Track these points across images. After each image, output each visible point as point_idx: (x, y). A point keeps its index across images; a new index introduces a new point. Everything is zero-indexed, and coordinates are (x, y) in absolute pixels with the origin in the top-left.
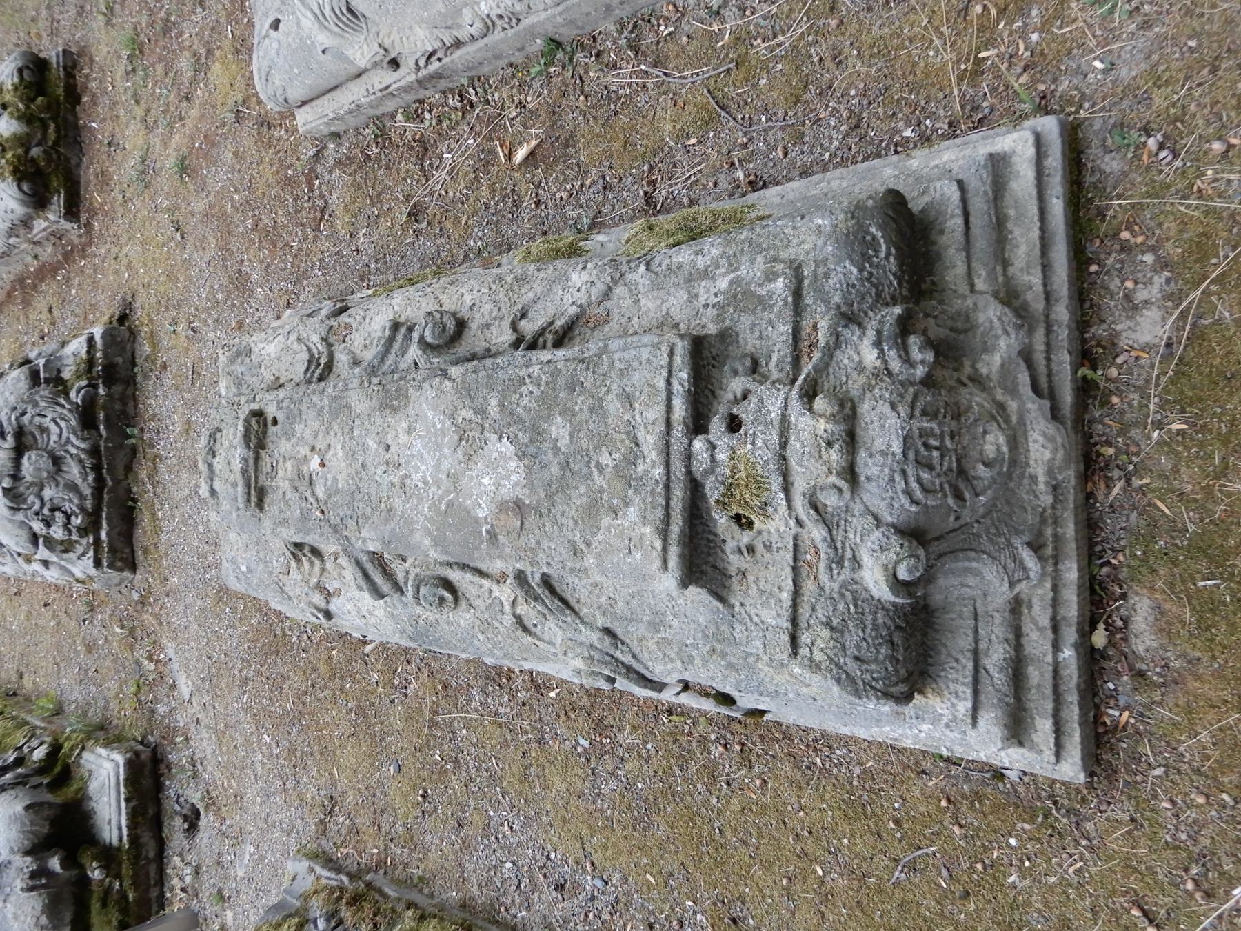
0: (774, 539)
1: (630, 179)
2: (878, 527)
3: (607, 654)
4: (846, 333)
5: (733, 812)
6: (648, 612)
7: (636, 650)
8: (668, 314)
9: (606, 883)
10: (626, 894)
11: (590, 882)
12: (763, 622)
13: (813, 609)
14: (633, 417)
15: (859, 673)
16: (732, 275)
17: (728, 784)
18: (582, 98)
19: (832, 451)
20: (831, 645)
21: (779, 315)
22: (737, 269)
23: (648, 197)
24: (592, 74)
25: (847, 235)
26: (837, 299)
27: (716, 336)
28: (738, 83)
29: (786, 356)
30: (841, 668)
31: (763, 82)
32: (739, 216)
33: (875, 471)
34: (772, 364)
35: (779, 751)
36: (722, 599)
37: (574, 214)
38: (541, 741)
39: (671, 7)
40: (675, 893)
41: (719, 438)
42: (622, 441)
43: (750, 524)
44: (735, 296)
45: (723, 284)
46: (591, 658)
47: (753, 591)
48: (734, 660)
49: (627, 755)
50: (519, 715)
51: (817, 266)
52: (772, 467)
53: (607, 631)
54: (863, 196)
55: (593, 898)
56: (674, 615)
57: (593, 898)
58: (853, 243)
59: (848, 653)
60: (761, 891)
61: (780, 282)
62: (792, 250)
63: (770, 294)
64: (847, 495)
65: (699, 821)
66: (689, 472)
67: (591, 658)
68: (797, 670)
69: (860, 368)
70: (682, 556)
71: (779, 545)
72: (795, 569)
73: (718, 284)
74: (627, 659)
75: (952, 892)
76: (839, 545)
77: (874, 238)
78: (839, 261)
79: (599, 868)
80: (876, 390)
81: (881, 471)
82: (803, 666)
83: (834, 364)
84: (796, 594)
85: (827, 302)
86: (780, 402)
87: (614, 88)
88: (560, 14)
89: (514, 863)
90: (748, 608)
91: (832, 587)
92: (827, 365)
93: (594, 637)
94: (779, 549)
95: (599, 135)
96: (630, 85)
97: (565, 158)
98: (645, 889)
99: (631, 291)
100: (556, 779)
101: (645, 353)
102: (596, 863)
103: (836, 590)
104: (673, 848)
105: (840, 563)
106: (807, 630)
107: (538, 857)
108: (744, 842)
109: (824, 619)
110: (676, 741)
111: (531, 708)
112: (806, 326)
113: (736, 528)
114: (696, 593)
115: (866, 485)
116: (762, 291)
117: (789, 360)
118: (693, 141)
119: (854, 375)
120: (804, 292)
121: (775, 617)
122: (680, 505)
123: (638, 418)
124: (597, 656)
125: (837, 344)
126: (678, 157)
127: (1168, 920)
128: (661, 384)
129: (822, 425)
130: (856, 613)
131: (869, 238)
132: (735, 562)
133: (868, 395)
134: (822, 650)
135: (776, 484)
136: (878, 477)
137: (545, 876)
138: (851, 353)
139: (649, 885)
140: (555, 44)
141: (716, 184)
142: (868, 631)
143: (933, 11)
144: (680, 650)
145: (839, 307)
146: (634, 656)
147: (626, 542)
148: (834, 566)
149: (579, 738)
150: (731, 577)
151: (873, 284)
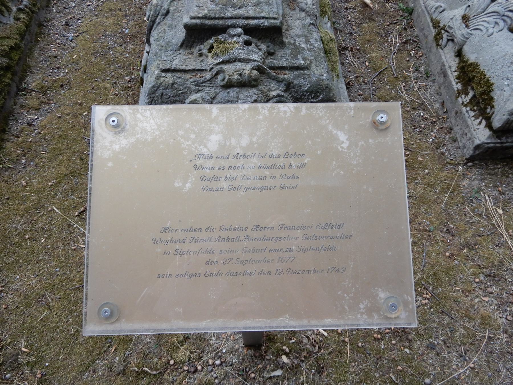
0: (205, 63)
1: (354, 42)
2: (211, 98)
3: (159, 13)
4: (283, 85)
5: (104, 85)
6: (176, 23)
7: (162, 23)
8: (293, 29)
9: (71, 41)
10: (68, 49)
11: (70, 35)
12: (174, 60)
13: (179, 78)
14: (250, 6)
15: (157, 95)
16: (306, 49)
17: (115, 83)
18: (388, 23)
19: (237, 76)
20: (166, 84)
21: (290, 62)
22: (309, 51)
23: (345, 49)
24: (398, 27)
25: (319, 85)
26: (295, 82)
27: (282, 40)
28: (389, 78)
29: (274, 64)
30: (158, 88)
31: (388, 87)
32: (334, 70)
33: (231, 94)
34: (271, 60)
35: (129, 100)
36: (181, 46)
37: (342, 22)
38: (126, 15)
39: (421, 54)
40: (70, 66)
41: (242, 38)
42: (241, 2)
43: (210, 52)
44: (298, 49)
45: (303, 45)
46: (157, 6)
47: (185, 57)
48: (159, 54)
49: (123, 47)
50: (136, 7)
51: (308, 75)
52: (231, 56)
53: (168, 12)
54: (334, 92)
55: (64, 37)
56: (175, 32)
57: (64, 37)
58: (316, 87)
59: (164, 91)
60: (75, 95)
61: (302, 62)
62: (314, 67)
63: (298, 59)
64: (222, 84)
65: (100, 73)
66: (229, 27)
67: (157, 6)
68: (156, 72)
69: (270, 90)
70: (196, 25)
71: (203, 65)
72: (194, 70)
73: (303, 44)
74: (158, 20)
75: (82, 156)
76: (204, 84)
77: (319, 96)
78: (310, 82)
79: (77, 38)
80: (261, 95)
81: (231, 97)
82: (158, 74)
83: (271, 81)
84: (185, 71)
85: (294, 79)
86: (256, 58)
87: (391, 36)
88: (422, 10)
89: (75, 7)
90: (179, 55)
91: (188, 84)
92: (270, 78)
93: (165, 6)
94: (202, 64)
95: (372, 30)
96: (392, 41)
97: (364, 18)
98: (70, 55)
99: (303, 18)
100: (111, 21)
101: (275, 10)
102: (79, 37)
103: (187, 86)
104: (88, 64)
105: (197, 85)
106: (172, 76)
107: (78, 16)
108: (93, 88)
109: (176, 81)
110: (130, 64)
111: (139, 12)
112: (286, 72)
113: (208, 47)
114: (181, 34)
115: (226, 92)
116: (299, 56)
117: (273, 65)
118: (367, 64)
119: (267, 88)
120: (298, 71)
121: (176, 64)
122: (216, 23)
123: (250, 8)
124: (158, 8)
125: (279, 82)
126: (361, 59)
127: (81, 218)
128: (262, 15)
129: (247, 72)
130: (179, 93)
131: (318, 94)
132: (196, 50)
133: (260, 92)
134: (164, 80)
135: (226, 58)
136: (229, 96)
137: (71, 18)
138: (275, 87)
139: (72, 56)
140: (411, 12)
141: (349, 72)
142: (173, 98)
143: (408, 140)
144: (162, 37)
145: (293, 83)
146: (159, 23)
147: (201, 5)
148: (196, 83)
149: (129, 30)
150: (190, 49)
151: (301, 96)
